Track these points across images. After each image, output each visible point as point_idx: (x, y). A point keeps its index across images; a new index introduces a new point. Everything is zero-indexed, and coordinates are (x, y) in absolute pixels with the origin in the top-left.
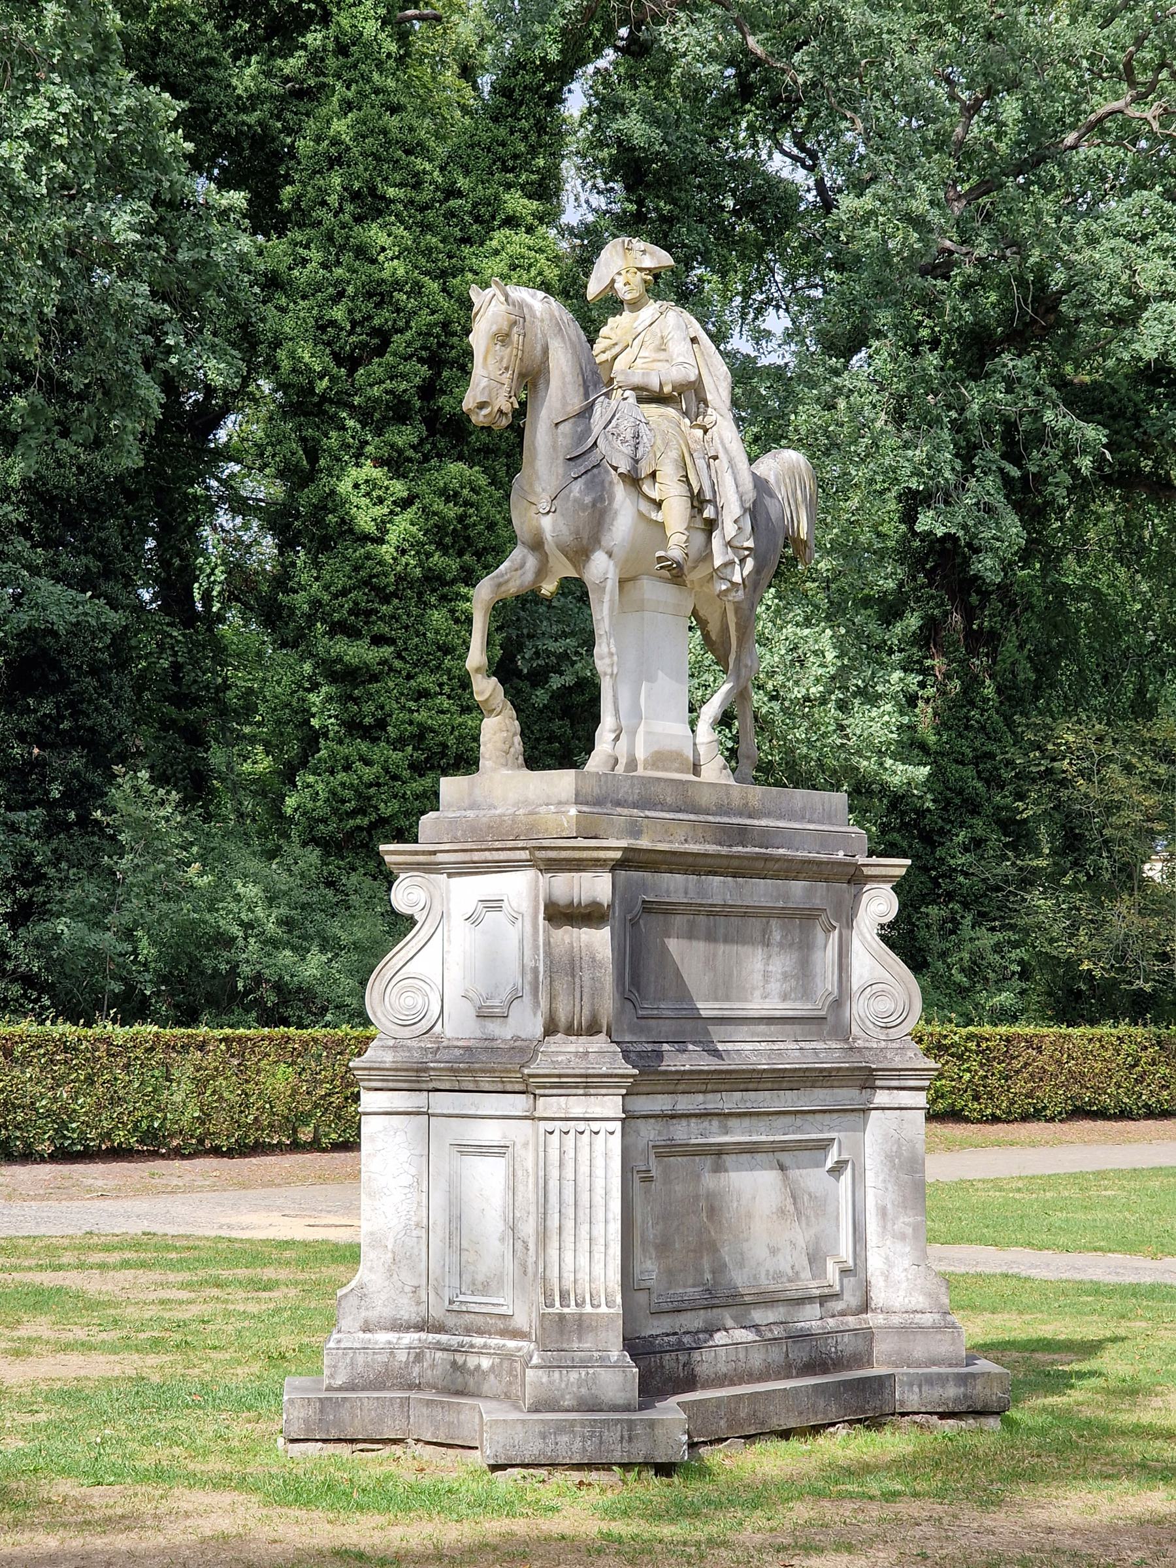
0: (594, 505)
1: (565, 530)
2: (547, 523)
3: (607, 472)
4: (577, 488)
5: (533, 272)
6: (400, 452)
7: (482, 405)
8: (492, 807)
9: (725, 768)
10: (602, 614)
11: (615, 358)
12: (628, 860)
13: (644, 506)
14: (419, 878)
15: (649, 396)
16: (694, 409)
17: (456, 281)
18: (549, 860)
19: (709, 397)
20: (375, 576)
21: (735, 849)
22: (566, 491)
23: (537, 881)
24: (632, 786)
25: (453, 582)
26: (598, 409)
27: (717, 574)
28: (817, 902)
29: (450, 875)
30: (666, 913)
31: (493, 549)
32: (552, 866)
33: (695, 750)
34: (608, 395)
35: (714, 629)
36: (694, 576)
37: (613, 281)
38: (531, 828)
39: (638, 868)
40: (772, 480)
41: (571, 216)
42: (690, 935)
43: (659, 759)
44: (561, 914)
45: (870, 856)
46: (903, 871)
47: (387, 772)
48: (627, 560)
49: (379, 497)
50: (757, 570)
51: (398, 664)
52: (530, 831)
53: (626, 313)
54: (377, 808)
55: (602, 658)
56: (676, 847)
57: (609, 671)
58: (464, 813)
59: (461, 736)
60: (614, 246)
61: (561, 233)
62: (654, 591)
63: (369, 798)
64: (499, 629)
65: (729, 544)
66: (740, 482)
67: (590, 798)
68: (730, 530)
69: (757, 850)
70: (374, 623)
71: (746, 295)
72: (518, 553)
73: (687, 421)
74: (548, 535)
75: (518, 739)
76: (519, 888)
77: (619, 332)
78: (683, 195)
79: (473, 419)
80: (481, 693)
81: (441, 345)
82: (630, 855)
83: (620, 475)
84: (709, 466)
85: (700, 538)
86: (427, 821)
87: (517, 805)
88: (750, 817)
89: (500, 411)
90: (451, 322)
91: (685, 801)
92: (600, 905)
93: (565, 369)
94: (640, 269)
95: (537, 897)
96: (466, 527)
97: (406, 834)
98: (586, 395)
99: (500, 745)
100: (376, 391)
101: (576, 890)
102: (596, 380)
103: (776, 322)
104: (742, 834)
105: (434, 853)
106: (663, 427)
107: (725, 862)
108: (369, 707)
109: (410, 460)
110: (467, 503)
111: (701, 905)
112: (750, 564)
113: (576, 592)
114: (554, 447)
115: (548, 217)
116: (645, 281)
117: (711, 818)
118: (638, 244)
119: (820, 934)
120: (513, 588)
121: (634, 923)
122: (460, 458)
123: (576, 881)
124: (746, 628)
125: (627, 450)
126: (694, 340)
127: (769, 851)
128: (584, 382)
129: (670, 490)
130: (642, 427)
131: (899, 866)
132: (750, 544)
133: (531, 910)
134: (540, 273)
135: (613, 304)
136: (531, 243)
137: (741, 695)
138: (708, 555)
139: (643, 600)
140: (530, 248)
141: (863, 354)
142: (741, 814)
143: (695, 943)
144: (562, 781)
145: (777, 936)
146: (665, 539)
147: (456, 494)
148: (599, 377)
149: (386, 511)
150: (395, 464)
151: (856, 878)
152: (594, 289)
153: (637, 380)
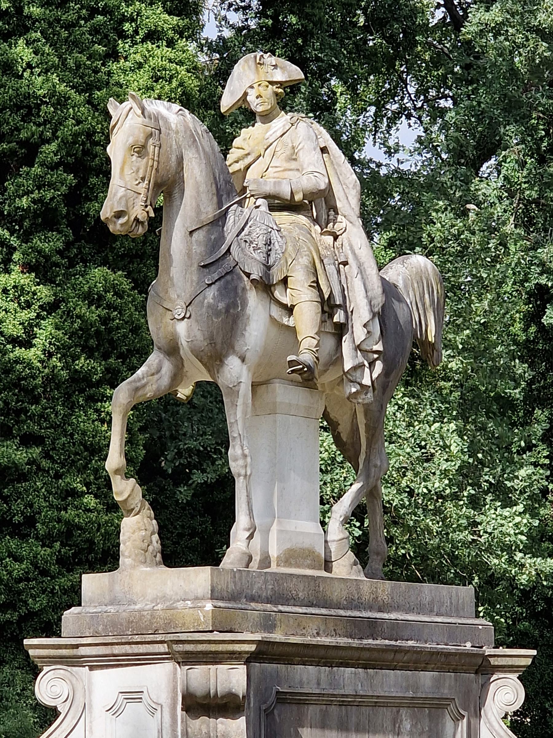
0: (227, 311)
1: (199, 336)
2: (182, 328)
3: (240, 278)
4: (211, 294)
5: (175, 83)
6: (47, 258)
7: (119, 214)
8: (132, 602)
9: (355, 564)
10: (237, 417)
11: (248, 168)
12: (263, 653)
13: (276, 312)
14: (61, 671)
15: (280, 204)
16: (324, 217)
17: (98, 94)
18: (187, 653)
19: (339, 205)
20: (24, 379)
21: (365, 642)
22: (200, 298)
23: (175, 673)
24: (266, 582)
25: (99, 383)
26: (231, 218)
27: (347, 377)
28: (446, 692)
29: (91, 668)
30: (299, 703)
31: (138, 352)
32: (189, 659)
33: (327, 547)
34: (240, 203)
35: (344, 430)
36: (325, 380)
37: (246, 94)
38: (169, 623)
39: (271, 660)
40: (400, 284)
41: (210, 32)
42: (323, 725)
43: (290, 557)
44: (199, 705)
45: (496, 647)
46: (529, 661)
47: (36, 567)
48: (259, 365)
49: (27, 301)
50: (386, 373)
51: (45, 464)
52: (169, 625)
53: (258, 125)
54: (26, 603)
55: (236, 460)
56: (308, 640)
57: (243, 472)
58: (104, 608)
59: (107, 532)
60: (246, 61)
61: (201, 47)
62: (285, 394)
63: (20, 593)
64: (142, 430)
65: (358, 348)
66: (369, 287)
67: (225, 594)
68: (360, 334)
69: (387, 642)
70: (24, 422)
71: (380, 106)
72: (154, 358)
73: (317, 227)
74: (183, 341)
75: (156, 537)
76: (159, 680)
77: (251, 142)
78: (317, 11)
79: (111, 228)
80: (120, 493)
81: (86, 152)
82: (264, 648)
83: (253, 281)
84: (339, 272)
85: (329, 343)
86: (69, 615)
87: (155, 600)
88: (380, 611)
89: (136, 220)
90: (95, 132)
91: (317, 596)
92: (235, 696)
93: (199, 178)
94: (272, 83)
95: (175, 689)
96: (110, 331)
97: (52, 629)
98: (220, 204)
99: (139, 543)
100: (24, 202)
101: (212, 681)
102: (228, 189)
103: (407, 133)
104: (372, 628)
105: (77, 646)
106: (295, 234)
107: (356, 654)
108: (18, 506)
109: (57, 265)
110: (110, 306)
111: (333, 695)
112: (379, 367)
113: (210, 396)
114: (189, 255)
115: (191, 31)
116: (277, 94)
117: (342, 612)
118: (270, 59)
119: (449, 724)
120: (149, 392)
121: (269, 713)
122: (104, 263)
123: (212, 673)
124: (375, 428)
125: (259, 256)
126: (324, 150)
127: (398, 643)
128: (218, 190)
129: (301, 295)
130: (274, 234)
131: (525, 656)
132: (379, 347)
133: (169, 701)
134: (181, 84)
135: (246, 115)
136: (172, 56)
137: (372, 492)
138: (337, 358)
139: (275, 403)
140: (170, 61)
141: (492, 161)
142: (371, 609)
143: (327, 733)
144: (199, 577)
145: (407, 725)
146: (297, 343)
147: (101, 298)
148: (232, 186)
149: (33, 315)
150: (41, 269)
151: (484, 669)
152: (227, 102)
153: (269, 189)
